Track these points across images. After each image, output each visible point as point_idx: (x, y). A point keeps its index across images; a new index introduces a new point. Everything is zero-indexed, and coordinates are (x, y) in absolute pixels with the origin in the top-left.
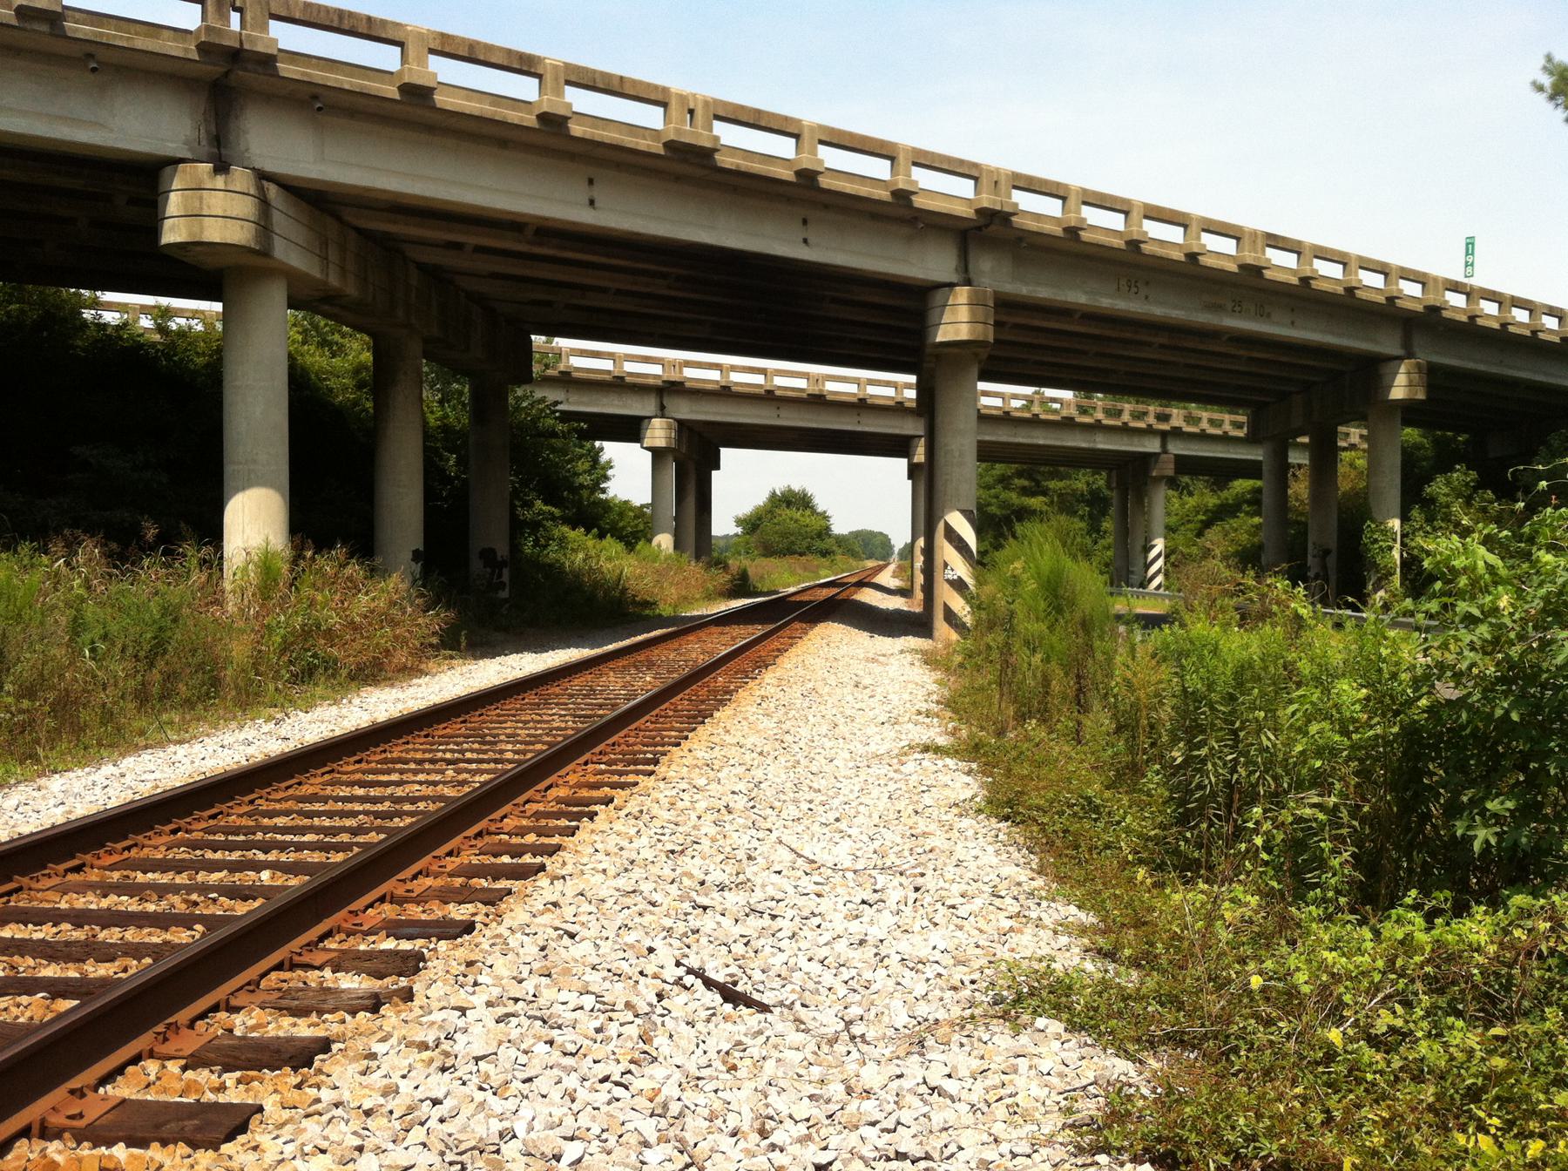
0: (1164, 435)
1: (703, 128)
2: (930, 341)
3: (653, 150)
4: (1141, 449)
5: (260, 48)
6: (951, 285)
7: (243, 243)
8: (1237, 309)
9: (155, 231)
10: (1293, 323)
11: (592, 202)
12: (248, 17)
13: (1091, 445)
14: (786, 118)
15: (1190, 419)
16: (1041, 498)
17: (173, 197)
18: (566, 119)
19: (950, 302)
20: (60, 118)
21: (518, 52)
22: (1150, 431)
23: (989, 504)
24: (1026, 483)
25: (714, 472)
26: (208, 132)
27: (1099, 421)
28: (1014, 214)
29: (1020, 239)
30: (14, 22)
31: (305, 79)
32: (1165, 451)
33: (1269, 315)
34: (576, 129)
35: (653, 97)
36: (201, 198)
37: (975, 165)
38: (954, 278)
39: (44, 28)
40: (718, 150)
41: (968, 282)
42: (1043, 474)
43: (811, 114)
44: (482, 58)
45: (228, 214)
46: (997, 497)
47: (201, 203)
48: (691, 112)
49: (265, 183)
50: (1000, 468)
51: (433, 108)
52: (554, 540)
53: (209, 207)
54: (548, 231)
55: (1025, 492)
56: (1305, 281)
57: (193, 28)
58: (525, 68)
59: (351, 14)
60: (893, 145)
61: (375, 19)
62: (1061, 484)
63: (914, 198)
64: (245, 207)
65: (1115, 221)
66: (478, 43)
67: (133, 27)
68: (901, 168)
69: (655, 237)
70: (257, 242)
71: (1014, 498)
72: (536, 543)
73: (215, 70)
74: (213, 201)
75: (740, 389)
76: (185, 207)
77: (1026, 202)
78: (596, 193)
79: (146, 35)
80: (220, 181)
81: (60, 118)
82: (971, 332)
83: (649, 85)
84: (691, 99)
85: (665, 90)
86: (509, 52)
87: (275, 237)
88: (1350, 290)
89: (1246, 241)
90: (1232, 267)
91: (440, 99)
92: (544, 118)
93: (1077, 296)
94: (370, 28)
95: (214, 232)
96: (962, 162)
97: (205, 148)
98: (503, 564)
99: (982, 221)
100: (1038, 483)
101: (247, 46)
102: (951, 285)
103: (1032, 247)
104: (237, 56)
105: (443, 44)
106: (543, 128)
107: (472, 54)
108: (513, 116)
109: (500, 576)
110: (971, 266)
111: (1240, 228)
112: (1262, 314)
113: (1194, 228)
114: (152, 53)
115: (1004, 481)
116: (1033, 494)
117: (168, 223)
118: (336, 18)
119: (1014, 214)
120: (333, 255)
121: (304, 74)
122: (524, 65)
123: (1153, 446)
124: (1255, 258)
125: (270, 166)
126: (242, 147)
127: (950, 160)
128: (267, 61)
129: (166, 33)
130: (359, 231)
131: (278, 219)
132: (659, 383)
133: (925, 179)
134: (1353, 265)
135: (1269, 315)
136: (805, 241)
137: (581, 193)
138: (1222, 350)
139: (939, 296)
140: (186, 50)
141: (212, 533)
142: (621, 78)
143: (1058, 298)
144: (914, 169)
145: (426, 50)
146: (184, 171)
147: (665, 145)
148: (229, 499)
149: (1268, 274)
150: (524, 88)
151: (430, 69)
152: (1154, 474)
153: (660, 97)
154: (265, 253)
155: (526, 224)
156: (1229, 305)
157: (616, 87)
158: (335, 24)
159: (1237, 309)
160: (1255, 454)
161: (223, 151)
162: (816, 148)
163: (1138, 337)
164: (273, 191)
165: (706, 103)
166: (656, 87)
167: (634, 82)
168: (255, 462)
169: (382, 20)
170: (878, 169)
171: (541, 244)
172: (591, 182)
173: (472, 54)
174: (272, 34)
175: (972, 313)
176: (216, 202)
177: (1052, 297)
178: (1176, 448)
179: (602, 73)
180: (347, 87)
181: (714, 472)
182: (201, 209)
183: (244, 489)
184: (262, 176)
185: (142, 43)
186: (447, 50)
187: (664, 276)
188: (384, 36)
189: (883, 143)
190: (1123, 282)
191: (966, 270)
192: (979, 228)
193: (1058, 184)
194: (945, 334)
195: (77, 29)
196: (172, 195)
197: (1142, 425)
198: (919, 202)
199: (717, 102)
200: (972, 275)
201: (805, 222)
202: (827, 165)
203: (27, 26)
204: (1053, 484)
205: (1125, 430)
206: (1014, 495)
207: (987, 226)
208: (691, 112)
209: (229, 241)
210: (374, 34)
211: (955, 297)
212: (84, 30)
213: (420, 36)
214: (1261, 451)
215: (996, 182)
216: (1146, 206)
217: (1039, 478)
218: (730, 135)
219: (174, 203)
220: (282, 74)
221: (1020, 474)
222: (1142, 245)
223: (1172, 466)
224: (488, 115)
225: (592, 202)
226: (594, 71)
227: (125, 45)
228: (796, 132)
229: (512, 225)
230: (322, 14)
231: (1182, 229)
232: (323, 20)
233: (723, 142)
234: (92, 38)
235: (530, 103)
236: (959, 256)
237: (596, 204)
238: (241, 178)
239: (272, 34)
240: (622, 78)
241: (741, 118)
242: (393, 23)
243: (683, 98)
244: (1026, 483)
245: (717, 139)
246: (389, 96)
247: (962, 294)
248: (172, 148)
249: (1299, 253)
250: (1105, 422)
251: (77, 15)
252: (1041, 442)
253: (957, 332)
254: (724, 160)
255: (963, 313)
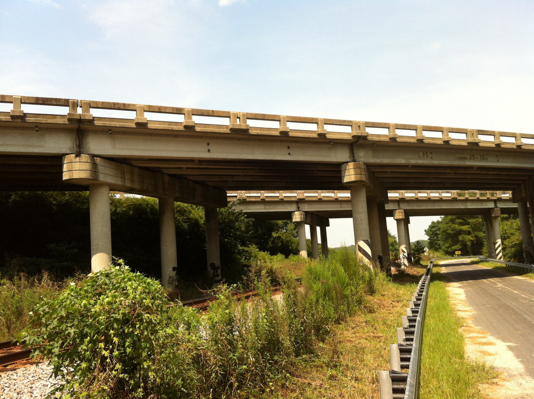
0: (495, 201)
1: (243, 123)
2: (343, 182)
3: (226, 132)
4: (486, 207)
5: (87, 118)
6: (347, 162)
7: (86, 177)
8: (472, 158)
9: (61, 177)
10: (498, 161)
11: (209, 151)
12: (138, 113)
13: (466, 207)
14: (275, 116)
15: (492, 195)
16: (467, 226)
17: (65, 166)
18: (288, 132)
19: (347, 168)
20: (29, 146)
21: (176, 108)
22: (488, 200)
23: (448, 230)
24: (461, 221)
25: (327, 228)
26: (76, 144)
27: (467, 198)
28: (424, 139)
29: (330, 142)
30: (11, 120)
31: (104, 125)
32: (496, 207)
33: (487, 159)
34: (198, 129)
35: (304, 121)
36: (72, 165)
37: (350, 122)
38: (348, 160)
39: (20, 120)
40: (368, 136)
41: (354, 161)
42: (467, 217)
43: (283, 113)
44: (163, 111)
45: (81, 169)
46: (450, 227)
47: (72, 167)
48: (359, 126)
49: (95, 158)
50: (450, 217)
51: (95, 125)
52: (252, 257)
53: (74, 168)
54: (201, 161)
55: (461, 224)
56: (498, 145)
57: (134, 118)
58: (178, 112)
59: (118, 104)
60: (317, 119)
61: (126, 104)
62: (474, 220)
63: (327, 135)
64: (87, 166)
65: (491, 138)
66: (162, 107)
67: (47, 117)
68: (320, 126)
69: (241, 159)
70: (91, 176)
71: (457, 227)
72: (246, 259)
73: (75, 126)
74: (75, 166)
75: (408, 199)
76: (68, 168)
77: (482, 138)
78: (210, 147)
79: (52, 118)
80: (78, 159)
81: (29, 146)
82: (355, 178)
83: (223, 112)
84: (238, 114)
85: (229, 113)
86: (173, 108)
87: (100, 174)
88: (519, 147)
89: (469, 134)
90: (465, 144)
91: (150, 126)
92: (319, 135)
93: (401, 161)
94: (124, 107)
95: (76, 175)
96: (345, 121)
97: (75, 149)
98: (218, 268)
99: (355, 140)
100: (465, 220)
101: (82, 118)
102: (347, 162)
103: (378, 146)
104: (80, 121)
105: (149, 109)
106: (186, 130)
107: (160, 110)
108: (175, 128)
109: (217, 272)
110: (355, 155)
111: (466, 130)
112: (483, 159)
113: (445, 132)
114: (54, 123)
115: (453, 221)
116: (464, 225)
117: (64, 173)
118: (113, 105)
119: (368, 136)
120: (127, 176)
121: (103, 123)
122: (178, 111)
123: (491, 205)
124: (356, 132)
125: (96, 153)
126: (88, 148)
127: (339, 121)
128: (91, 121)
129: (58, 117)
130: (140, 168)
131: (100, 168)
132: (398, 199)
133: (453, 136)
134: (518, 137)
135: (487, 159)
136: (289, 154)
137: (205, 148)
138: (475, 172)
139: (343, 167)
140: (64, 121)
141: (88, 268)
142: (213, 111)
143: (392, 162)
144: (522, 139)
145: (236, 117)
146: (67, 157)
147: (467, 143)
148: (93, 256)
149: (481, 144)
150: (275, 125)
151: (91, 113)
152: (493, 216)
153: (227, 115)
154: (96, 180)
155: (408, 166)
156: (469, 157)
157: (211, 113)
158: (113, 107)
159: (472, 158)
160: (515, 205)
161: (79, 150)
162: (422, 132)
163: (437, 171)
164: (98, 160)
165: (244, 115)
166: (226, 112)
167: (217, 112)
168: (98, 245)
169: (128, 104)
170: (313, 127)
171: (201, 165)
172: (208, 144)
173: (160, 110)
174: (367, 131)
175: (355, 171)
176: (77, 166)
177: (390, 162)
178: (500, 205)
179: (205, 110)
180: (118, 126)
181: (327, 228)
182: (72, 168)
183: (95, 254)
184: (93, 156)
185: (50, 121)
186: (151, 110)
187: (254, 169)
188: (129, 109)
189: (312, 119)
190: (421, 153)
191: (354, 157)
192: (355, 142)
193: (385, 124)
194: (347, 179)
195: (30, 120)
196: (65, 165)
197: (485, 198)
198: (328, 136)
199: (247, 114)
200: (356, 158)
201: (288, 148)
202: (290, 129)
203: (15, 121)
204: (471, 221)
205: (478, 200)
206: (457, 226)
207: (358, 141)
208: (359, 126)
209: (81, 177)
210: (165, 111)
211: (349, 166)
212: (32, 119)
213: (321, 120)
214: (516, 204)
215: (473, 134)
216: (521, 134)
217: (465, 218)
218: (370, 131)
219: (65, 167)
220: (96, 125)
221: (458, 218)
222: (479, 144)
223: (500, 212)
224: (167, 128)
225: (209, 151)
226: (203, 110)
227: (45, 122)
228: (279, 119)
229: (191, 160)
230: (108, 105)
231: (441, 133)
232: (108, 106)
233: (369, 133)
234: (35, 122)
235: (277, 129)
236: (350, 152)
237: (210, 151)
238: (84, 157)
239: (367, 131)
240: (213, 111)
241: (257, 118)
242: (132, 104)
243: (356, 123)
244: (461, 221)
245: (248, 125)
246: (132, 127)
247: (351, 165)
248: (64, 151)
249: (494, 136)
250: (470, 198)
251: (30, 115)
252: (445, 208)
253: (350, 178)
254: (252, 132)
255: (352, 172)
